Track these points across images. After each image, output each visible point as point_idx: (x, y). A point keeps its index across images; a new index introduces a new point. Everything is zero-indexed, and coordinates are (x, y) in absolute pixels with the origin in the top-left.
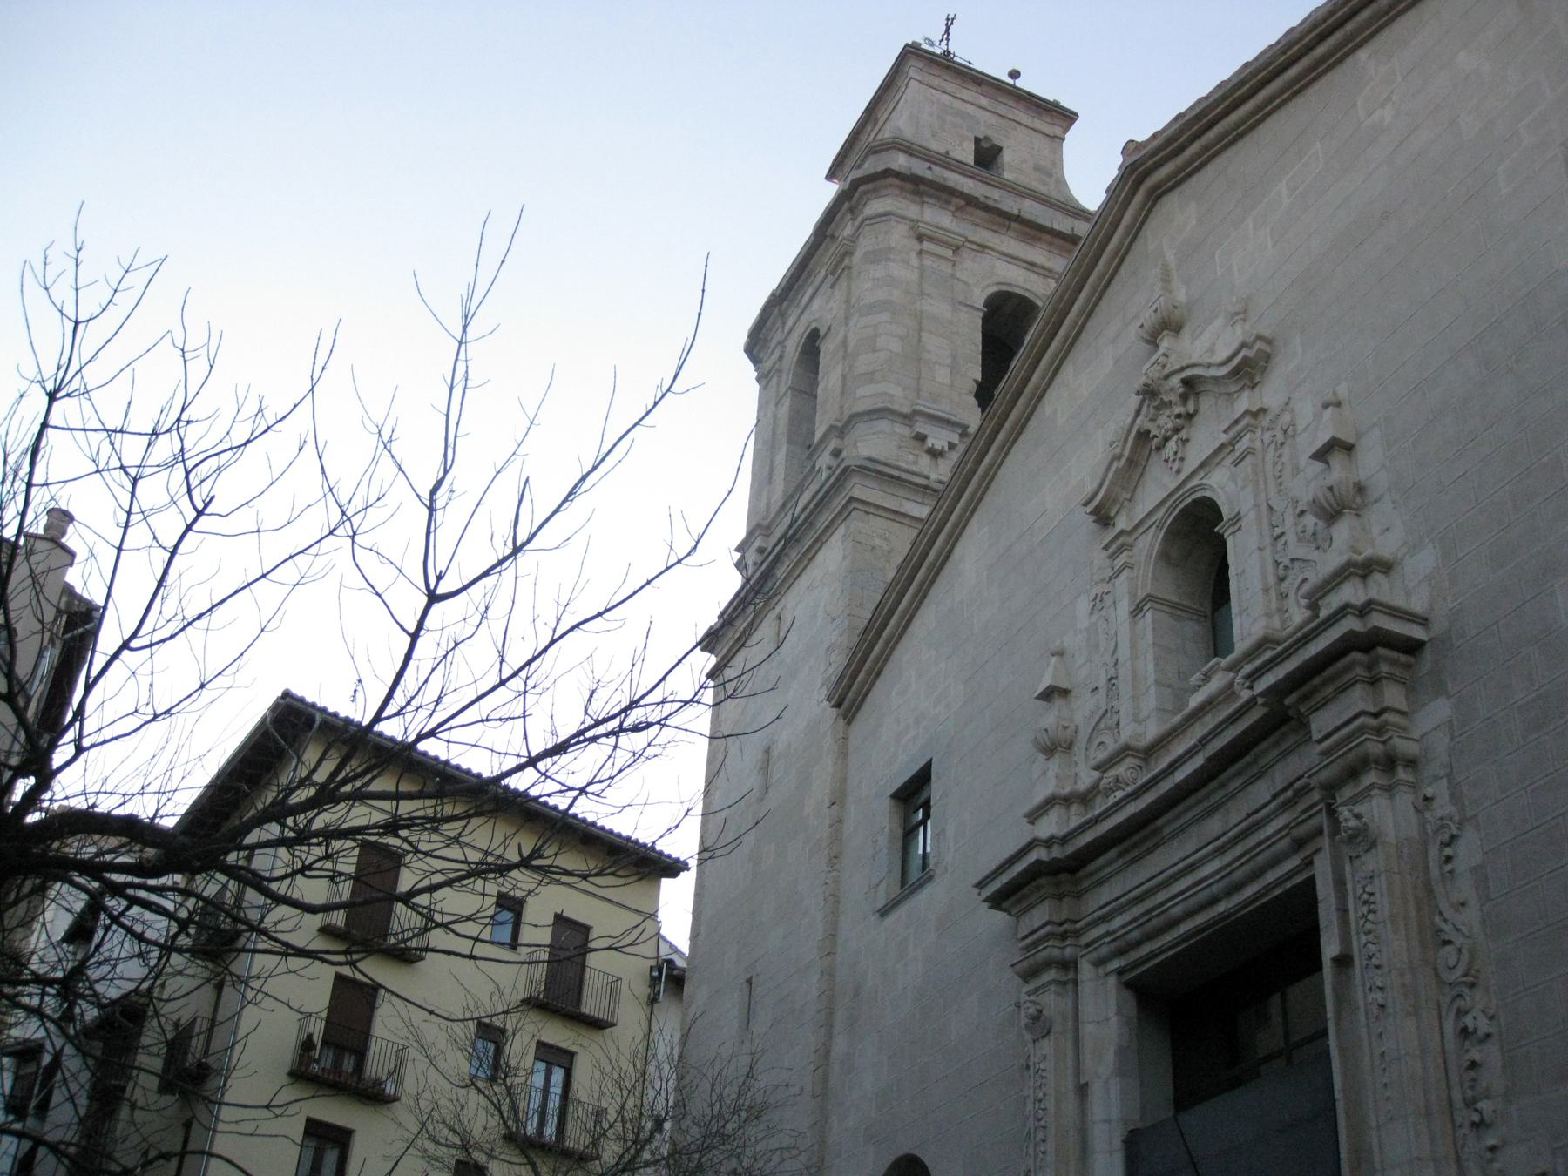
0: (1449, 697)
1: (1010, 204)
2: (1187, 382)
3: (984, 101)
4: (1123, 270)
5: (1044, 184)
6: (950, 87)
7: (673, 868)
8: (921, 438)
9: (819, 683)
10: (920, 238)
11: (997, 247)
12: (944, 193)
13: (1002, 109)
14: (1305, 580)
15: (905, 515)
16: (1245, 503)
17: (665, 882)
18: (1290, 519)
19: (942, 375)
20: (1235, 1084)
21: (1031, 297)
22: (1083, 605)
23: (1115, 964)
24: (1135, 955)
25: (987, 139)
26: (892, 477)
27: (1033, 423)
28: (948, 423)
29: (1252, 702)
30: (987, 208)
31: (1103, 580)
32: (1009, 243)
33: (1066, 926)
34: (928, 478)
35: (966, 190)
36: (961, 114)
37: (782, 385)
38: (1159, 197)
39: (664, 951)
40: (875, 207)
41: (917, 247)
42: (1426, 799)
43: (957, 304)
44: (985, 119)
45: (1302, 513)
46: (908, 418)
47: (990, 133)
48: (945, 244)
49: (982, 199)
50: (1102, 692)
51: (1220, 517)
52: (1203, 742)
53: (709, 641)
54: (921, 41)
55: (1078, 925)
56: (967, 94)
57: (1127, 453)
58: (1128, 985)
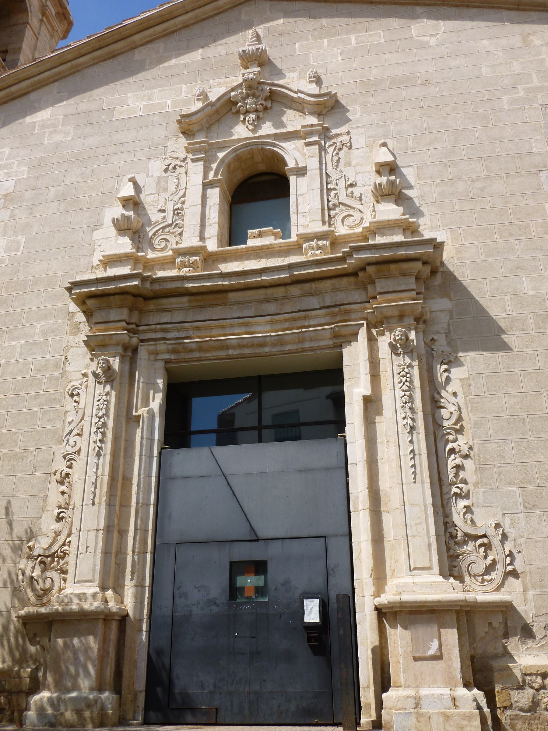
0: (451, 300)
23: (167, 356)
27: (120, 58)
55: (141, 328)
57: (218, 105)
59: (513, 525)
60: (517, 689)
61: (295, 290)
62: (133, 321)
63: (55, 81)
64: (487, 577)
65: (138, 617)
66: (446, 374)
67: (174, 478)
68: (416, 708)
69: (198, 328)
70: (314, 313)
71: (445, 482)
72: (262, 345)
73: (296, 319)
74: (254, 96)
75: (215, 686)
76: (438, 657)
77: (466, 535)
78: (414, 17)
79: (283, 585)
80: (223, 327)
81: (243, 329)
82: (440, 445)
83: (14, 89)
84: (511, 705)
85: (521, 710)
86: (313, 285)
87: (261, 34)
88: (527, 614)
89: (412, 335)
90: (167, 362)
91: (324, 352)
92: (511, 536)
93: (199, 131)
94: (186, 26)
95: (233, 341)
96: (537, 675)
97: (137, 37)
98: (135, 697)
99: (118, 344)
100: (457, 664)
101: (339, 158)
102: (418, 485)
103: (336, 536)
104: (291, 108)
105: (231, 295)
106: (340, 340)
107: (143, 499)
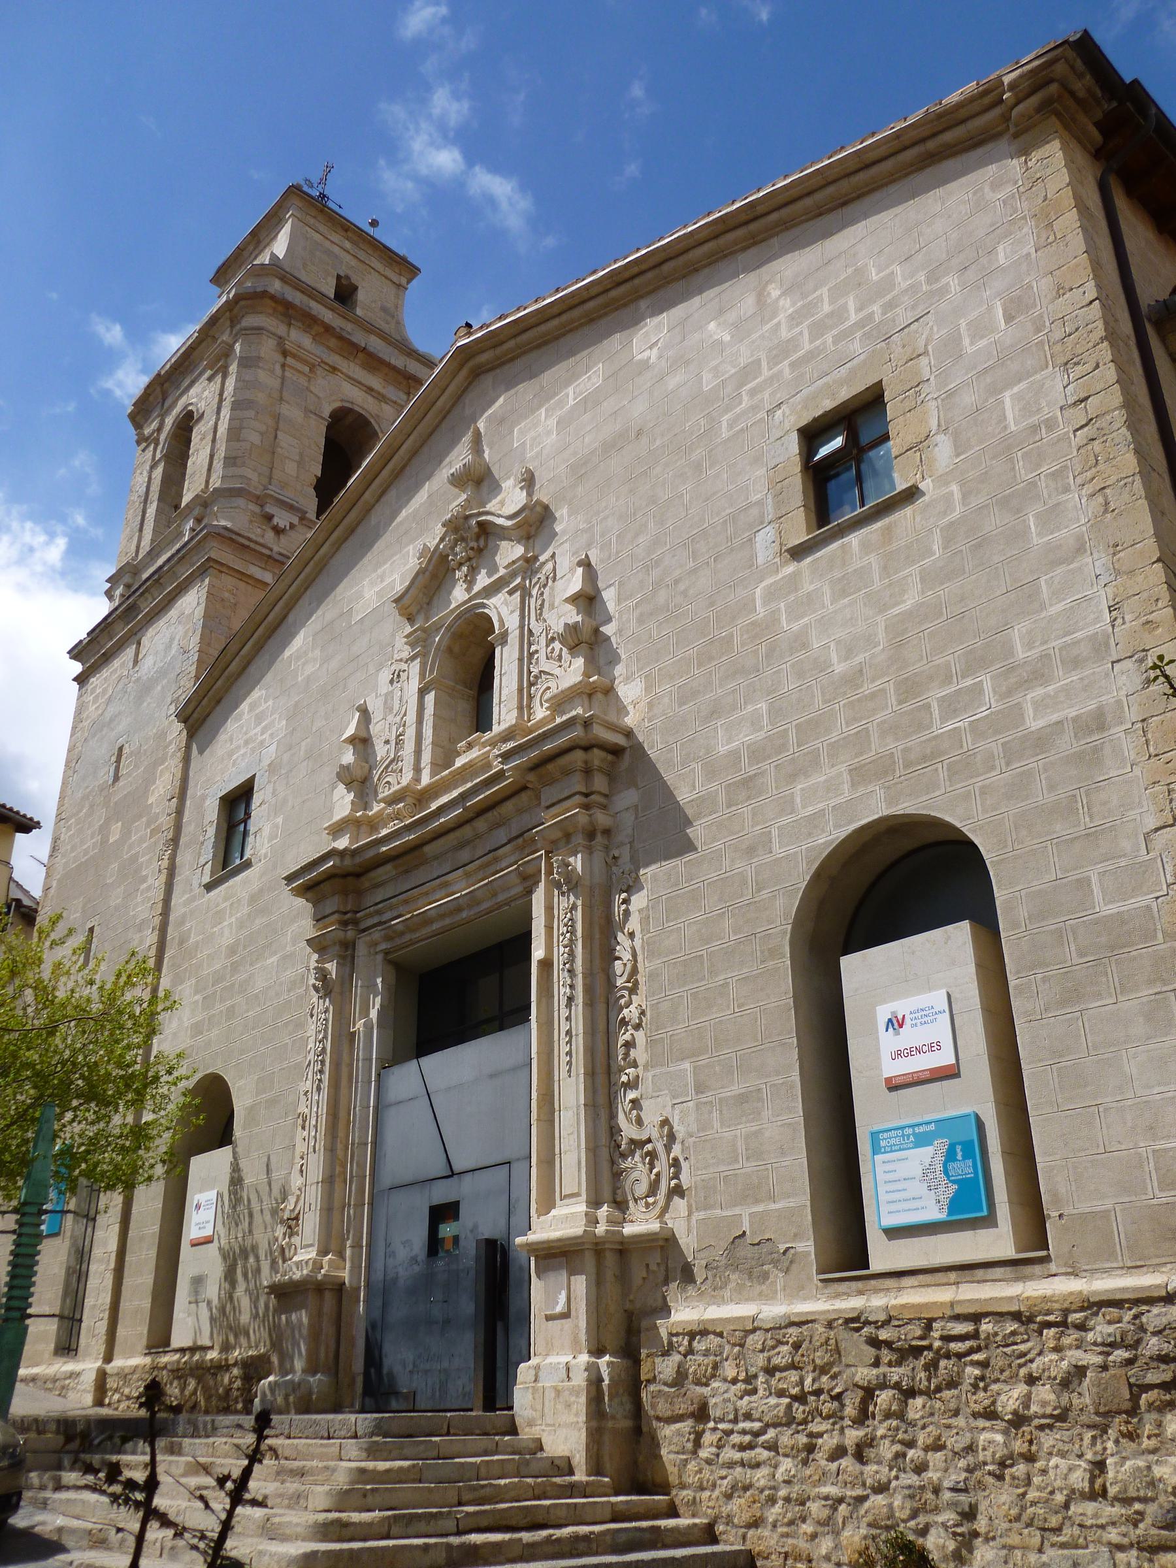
0: (638, 789)
1: (359, 338)
2: (481, 524)
3: (348, 245)
4: (443, 425)
5: (388, 323)
6: (322, 228)
7: (26, 825)
8: (269, 518)
9: (169, 700)
10: (285, 353)
11: (344, 370)
12: (309, 321)
13: (362, 255)
14: (549, 688)
15: (250, 577)
16: (512, 622)
17: (19, 836)
18: (543, 642)
19: (291, 468)
20: (531, 378)
21: (367, 415)
22: (385, 676)
23: (383, 946)
24: (398, 941)
25: (347, 277)
26: (243, 545)
27: (359, 530)
28: (291, 508)
29: (500, 775)
30: (341, 338)
31: (401, 660)
32: (355, 370)
33: (349, 916)
34: (271, 550)
35: (326, 320)
36: (328, 253)
37: (158, 451)
38: (478, 375)
39: (16, 894)
40: (250, 321)
41: (281, 359)
42: (614, 858)
43: (307, 411)
44: (347, 260)
45: (553, 639)
46: (260, 500)
47: (350, 273)
48: (305, 362)
49: (338, 330)
50: (393, 743)
51: (491, 630)
52: (463, 797)
53: (77, 653)
54: (302, 183)
55: (358, 915)
56: (335, 237)
57: (431, 568)
58: (390, 962)
59: (681, 1121)
60: (662, 1355)
61: (481, 824)
62: (349, 908)
63: (306, 589)
64: (651, 1200)
65: (355, 1285)
66: (624, 907)
67: (390, 1105)
68: (535, 1381)
69: (406, 902)
70: (501, 851)
71: (614, 1069)
72: (459, 910)
73: (488, 865)
74: (463, 539)
75: (414, 1365)
76: (566, 1315)
77: (632, 1141)
78: (636, 321)
79: (472, 1231)
80: (427, 894)
81: (443, 892)
82: (612, 1015)
83: (270, 618)
84: (655, 1377)
85: (665, 1384)
86: (495, 812)
87: (482, 430)
88: (688, 1248)
89: (577, 862)
90: (387, 953)
91: (518, 902)
92: (680, 1136)
93: (418, 612)
94: (414, 453)
95: (432, 912)
96: (684, 1334)
97: (367, 495)
98: (353, 1382)
99: (335, 944)
100: (583, 1324)
101: (543, 600)
102: (573, 1079)
103: (518, 1160)
104: (505, 539)
105: (427, 849)
106: (529, 883)
107: (360, 1138)
